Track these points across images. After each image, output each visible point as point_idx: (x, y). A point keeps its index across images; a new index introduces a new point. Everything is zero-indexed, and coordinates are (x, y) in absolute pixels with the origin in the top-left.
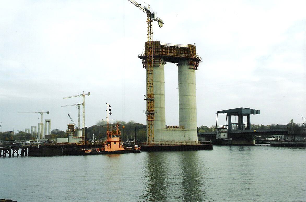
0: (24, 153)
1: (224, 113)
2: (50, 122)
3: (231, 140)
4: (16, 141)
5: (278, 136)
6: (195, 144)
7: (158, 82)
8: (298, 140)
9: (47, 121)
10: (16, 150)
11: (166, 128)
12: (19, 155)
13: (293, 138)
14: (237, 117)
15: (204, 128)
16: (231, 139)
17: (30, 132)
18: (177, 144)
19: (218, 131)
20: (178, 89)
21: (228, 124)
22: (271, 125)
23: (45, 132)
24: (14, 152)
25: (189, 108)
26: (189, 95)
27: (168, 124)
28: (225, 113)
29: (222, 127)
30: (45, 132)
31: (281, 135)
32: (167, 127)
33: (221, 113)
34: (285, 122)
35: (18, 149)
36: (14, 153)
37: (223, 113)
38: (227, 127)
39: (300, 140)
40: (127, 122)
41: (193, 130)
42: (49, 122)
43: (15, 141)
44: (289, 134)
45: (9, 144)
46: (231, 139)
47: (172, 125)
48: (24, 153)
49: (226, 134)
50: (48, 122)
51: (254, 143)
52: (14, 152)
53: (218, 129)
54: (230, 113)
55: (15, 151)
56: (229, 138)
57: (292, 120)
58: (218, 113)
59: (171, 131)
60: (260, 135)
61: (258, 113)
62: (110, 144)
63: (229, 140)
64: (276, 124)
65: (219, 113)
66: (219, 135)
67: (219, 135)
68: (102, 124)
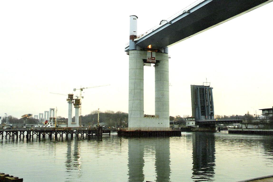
0: (29, 134)
2: (54, 111)
4: (26, 125)
5: (236, 125)
6: (167, 130)
7: (132, 79)
8: (250, 128)
9: (51, 110)
10: (22, 132)
11: (144, 117)
12: (24, 136)
13: (246, 126)
15: (171, 116)
16: (198, 126)
17: (38, 119)
18: (153, 129)
19: (188, 120)
22: (231, 116)
24: (21, 133)
27: (146, 113)
31: (239, 124)
32: (146, 116)
34: (242, 113)
35: (24, 131)
36: (21, 134)
39: (251, 128)
40: (115, 112)
41: (166, 118)
42: (53, 110)
43: (26, 125)
44: (243, 122)
45: (21, 127)
46: (198, 126)
48: (29, 134)
49: (194, 122)
50: (52, 110)
51: (217, 130)
52: (21, 133)
55: (8, 134)
57: (248, 113)
61: (263, 111)
62: (19, 131)
63: (197, 127)
64: (235, 115)
66: (188, 123)
67: (188, 123)
68: (113, 113)
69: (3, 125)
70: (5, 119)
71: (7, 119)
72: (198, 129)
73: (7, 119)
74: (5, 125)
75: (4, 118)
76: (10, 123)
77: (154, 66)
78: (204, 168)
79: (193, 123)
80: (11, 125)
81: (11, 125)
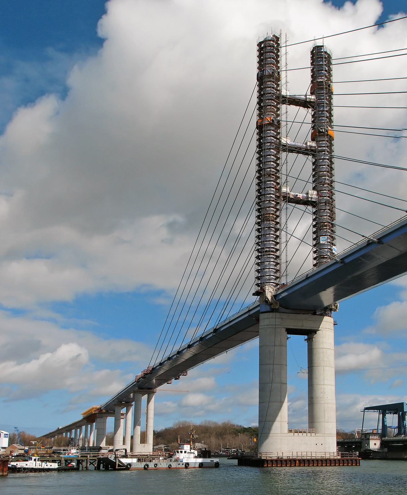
14: (396, 416)
16: (386, 450)
23: (396, 430)
26: (325, 403)
28: (377, 411)
29: (372, 431)
30: (396, 430)
37: (373, 411)
38: (380, 432)
47: (310, 59)
53: (366, 437)
54: (384, 410)
56: (383, 449)
58: (366, 411)
59: (280, 268)
60: (104, 412)
63: (383, 452)
65: (367, 411)
69: (12, 450)
70: (12, 438)
71: (17, 437)
72: (386, 455)
73: (17, 437)
74: (16, 448)
75: (11, 435)
76: (25, 446)
77: (306, 340)
78: (121, 464)
79: (375, 444)
80: (27, 448)
81: (27, 448)
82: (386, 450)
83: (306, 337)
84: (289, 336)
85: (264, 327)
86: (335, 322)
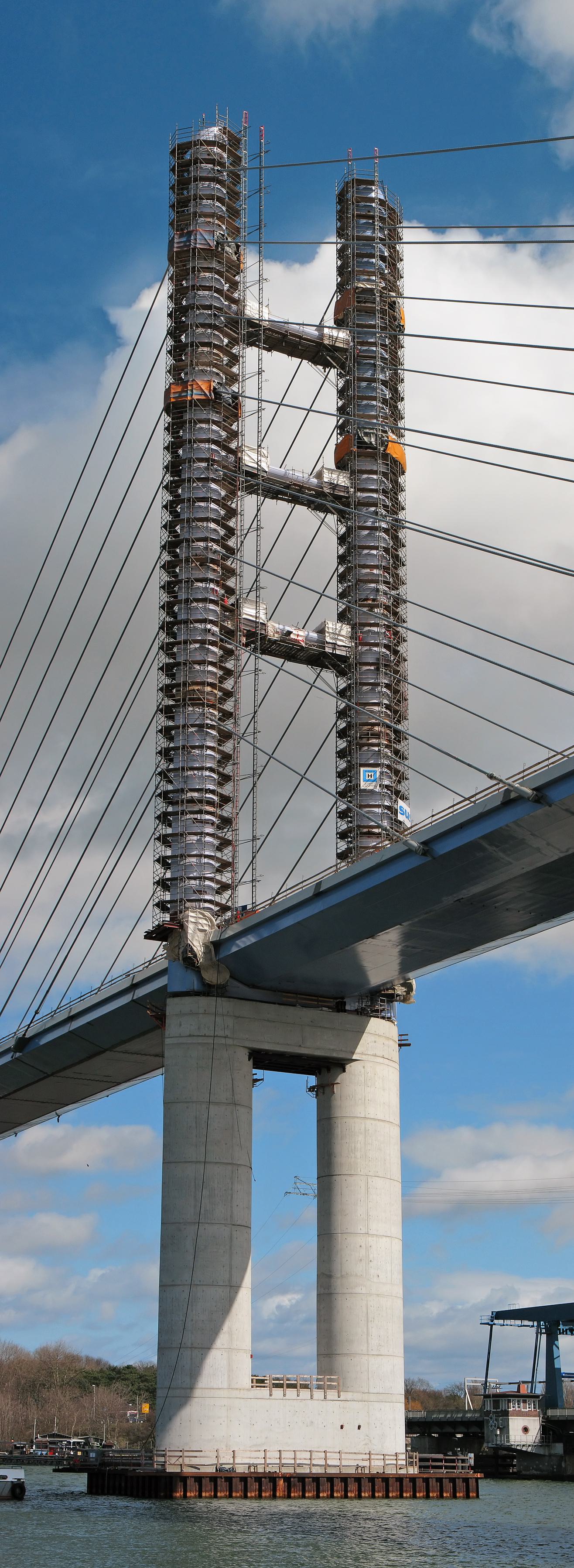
1: (526, 1323)
3: (555, 1455)
16: (559, 1448)
20: (403, 1359)
21: (541, 1375)
25: (364, 1291)
26: (485, 1384)
28: (531, 1323)
33: (508, 1322)
37: (518, 1322)
38: (540, 1389)
56: (548, 1446)
58: (496, 1321)
63: (550, 1456)
65: (501, 1322)
82: (559, 1448)
83: (312, 1080)
84: (259, 1073)
85: (181, 1040)
86: (403, 1038)
